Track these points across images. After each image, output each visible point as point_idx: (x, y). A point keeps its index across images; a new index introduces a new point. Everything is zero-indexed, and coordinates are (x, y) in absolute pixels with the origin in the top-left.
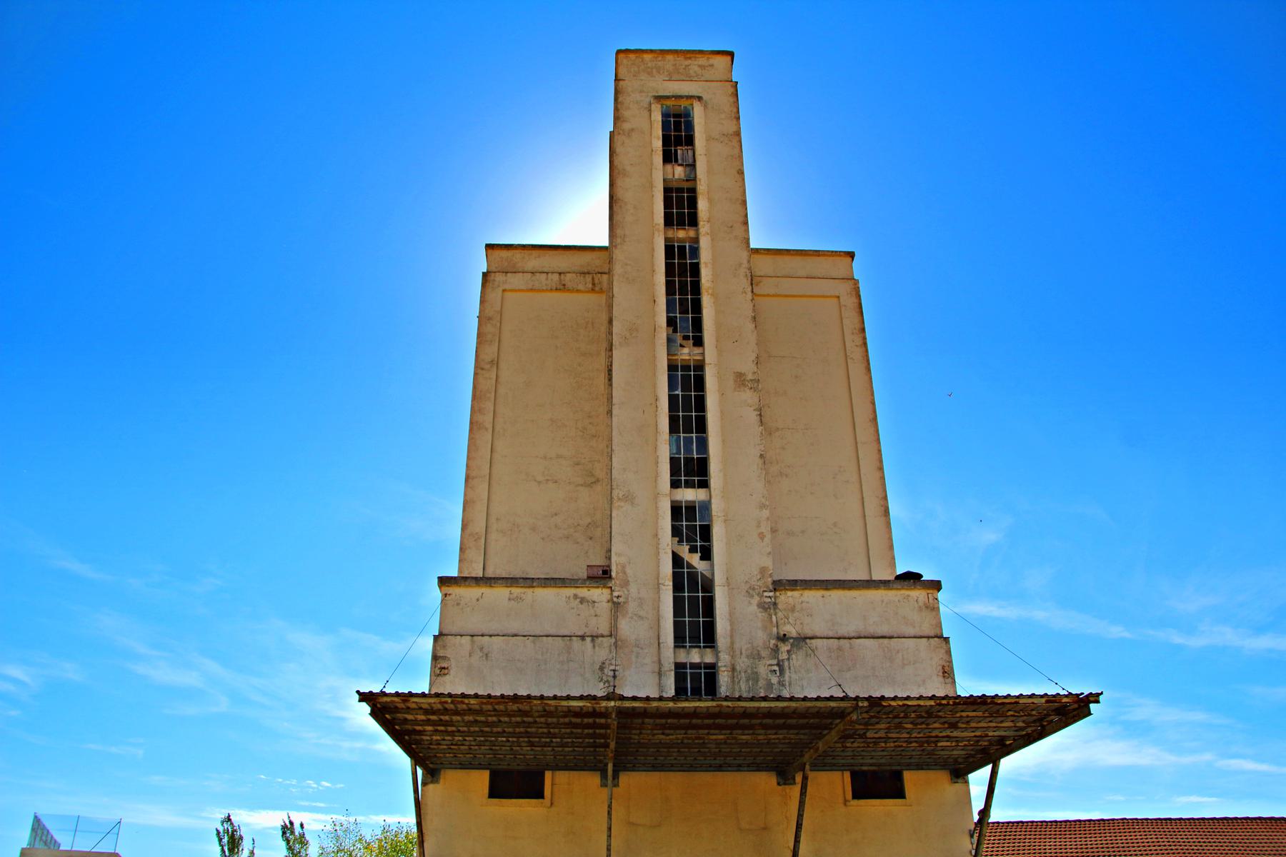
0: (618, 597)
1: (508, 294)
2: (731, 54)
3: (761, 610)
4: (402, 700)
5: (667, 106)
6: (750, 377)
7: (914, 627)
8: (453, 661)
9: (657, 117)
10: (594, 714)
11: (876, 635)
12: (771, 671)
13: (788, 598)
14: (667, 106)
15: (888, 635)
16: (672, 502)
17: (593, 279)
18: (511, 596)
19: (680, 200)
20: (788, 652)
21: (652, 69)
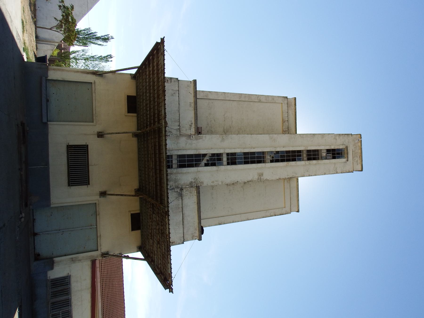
0: (192, 137)
1: (281, 104)
2: (362, 170)
3: (190, 182)
4: (162, 53)
5: (344, 150)
6: (262, 178)
7: (187, 232)
8: (170, 84)
9: (341, 147)
10: (159, 120)
11: (184, 220)
12: (171, 186)
13: (195, 192)
14: (344, 150)
15: (184, 224)
16: (222, 153)
17: (287, 131)
18: (191, 103)
19: (315, 155)
20: (177, 191)
21: (356, 145)
